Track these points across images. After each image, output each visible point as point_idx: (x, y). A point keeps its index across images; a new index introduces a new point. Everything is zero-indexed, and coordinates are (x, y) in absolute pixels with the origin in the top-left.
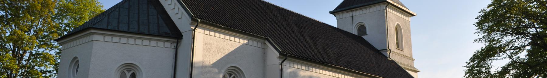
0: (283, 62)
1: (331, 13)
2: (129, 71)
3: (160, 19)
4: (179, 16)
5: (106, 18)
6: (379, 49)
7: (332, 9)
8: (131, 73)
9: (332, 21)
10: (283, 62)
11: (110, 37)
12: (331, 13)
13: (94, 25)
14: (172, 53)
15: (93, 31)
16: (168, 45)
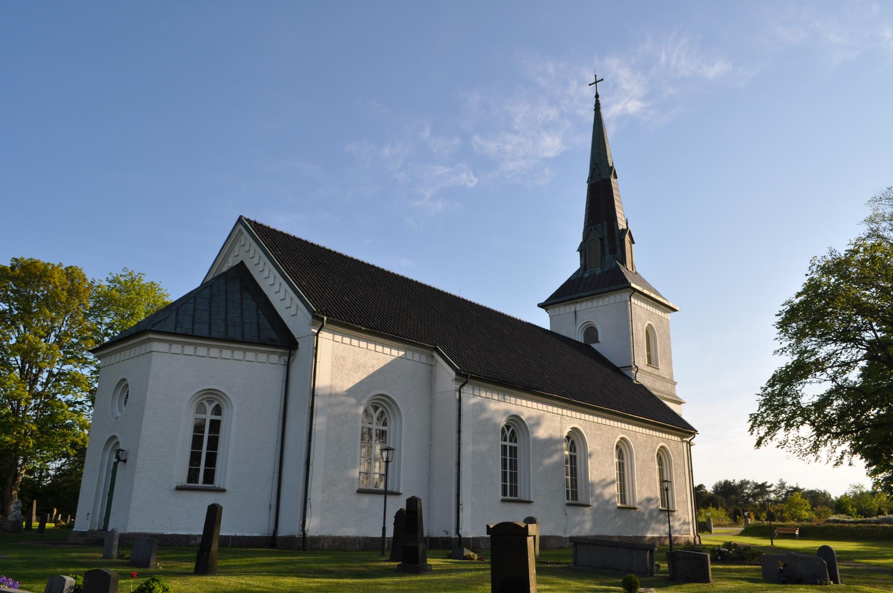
0: (461, 387)
1: (541, 306)
2: (210, 401)
3: (262, 317)
4: (293, 311)
5: (174, 315)
6: (618, 366)
7: (543, 300)
8: (214, 405)
9: (542, 320)
10: (461, 387)
11: (180, 346)
12: (541, 306)
13: (153, 326)
14: (280, 372)
15: (151, 336)
16: (274, 358)
